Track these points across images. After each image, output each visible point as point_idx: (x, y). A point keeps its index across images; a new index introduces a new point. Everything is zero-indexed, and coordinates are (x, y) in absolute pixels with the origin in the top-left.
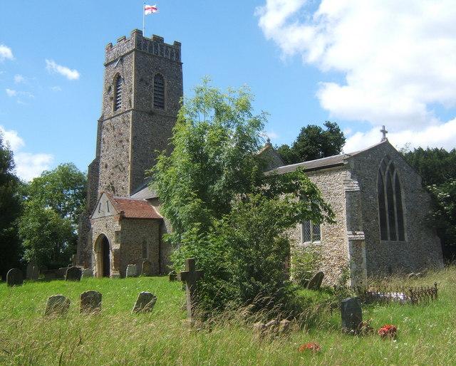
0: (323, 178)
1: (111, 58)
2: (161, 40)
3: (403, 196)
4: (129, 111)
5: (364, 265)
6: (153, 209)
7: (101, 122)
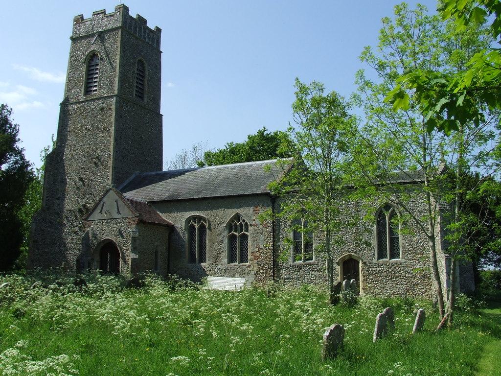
2: (145, 21)
4: (111, 97)
6: (158, 215)
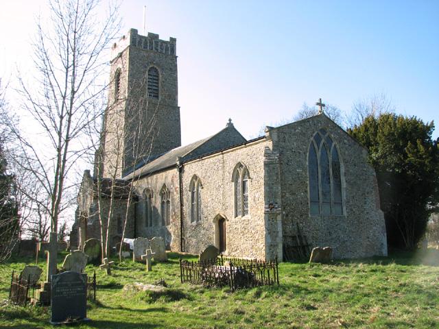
2: (157, 36)
3: (343, 170)
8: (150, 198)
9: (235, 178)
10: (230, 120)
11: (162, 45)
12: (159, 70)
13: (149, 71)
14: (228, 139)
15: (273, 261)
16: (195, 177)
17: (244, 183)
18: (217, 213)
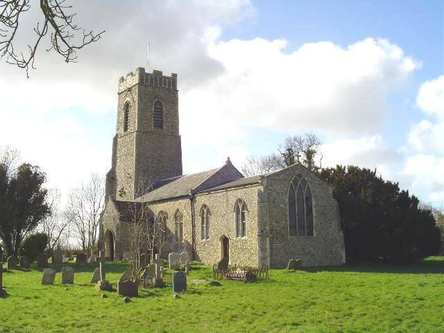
0: (154, 205)
1: (122, 88)
2: (160, 73)
5: (268, 254)
7: (115, 139)
8: (165, 219)
9: (237, 210)
10: (228, 158)
11: (165, 81)
12: (163, 104)
13: (155, 105)
14: (226, 177)
15: (263, 268)
16: (205, 206)
17: (243, 214)
18: (222, 234)
